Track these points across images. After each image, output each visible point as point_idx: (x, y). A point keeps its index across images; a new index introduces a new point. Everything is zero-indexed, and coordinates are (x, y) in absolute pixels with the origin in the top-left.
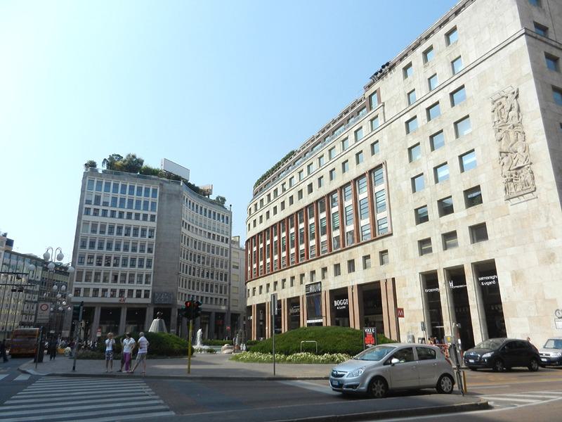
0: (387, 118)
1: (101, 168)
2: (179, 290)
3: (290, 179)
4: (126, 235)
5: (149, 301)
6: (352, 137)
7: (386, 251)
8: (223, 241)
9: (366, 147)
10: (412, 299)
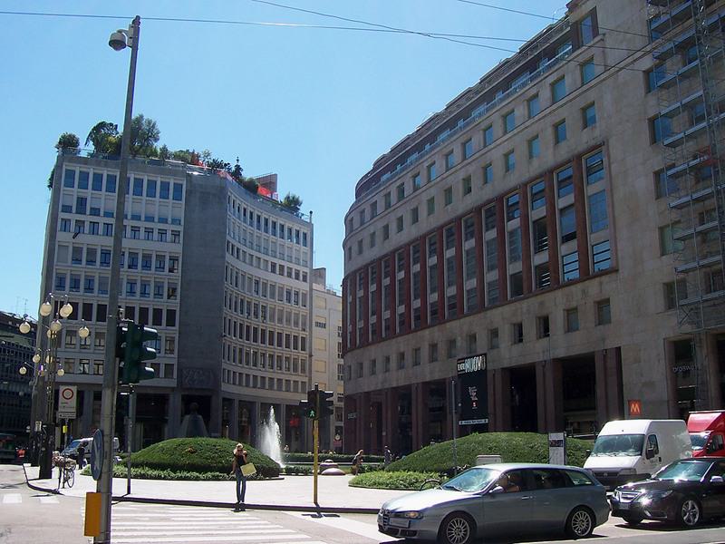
0: (534, 192)
1: (86, 149)
2: (224, 366)
3: (429, 167)
4: (129, 267)
5: (173, 383)
6: (545, 94)
7: (608, 301)
8: (147, 258)
9: (570, 113)
10: (650, 385)
